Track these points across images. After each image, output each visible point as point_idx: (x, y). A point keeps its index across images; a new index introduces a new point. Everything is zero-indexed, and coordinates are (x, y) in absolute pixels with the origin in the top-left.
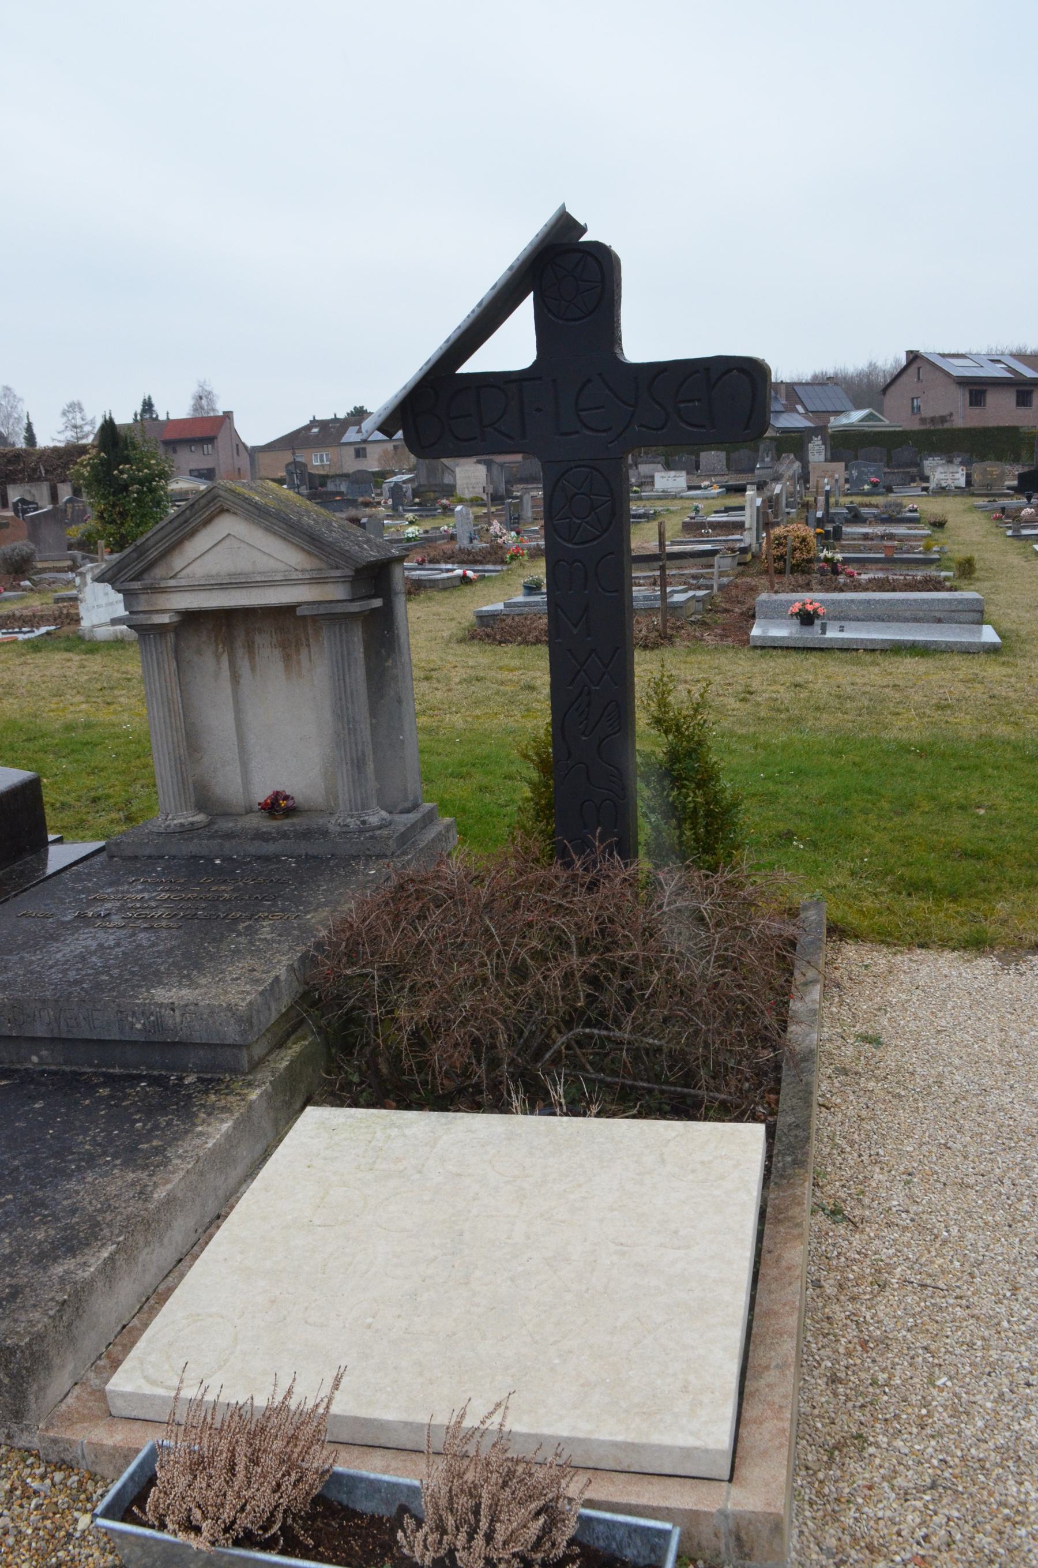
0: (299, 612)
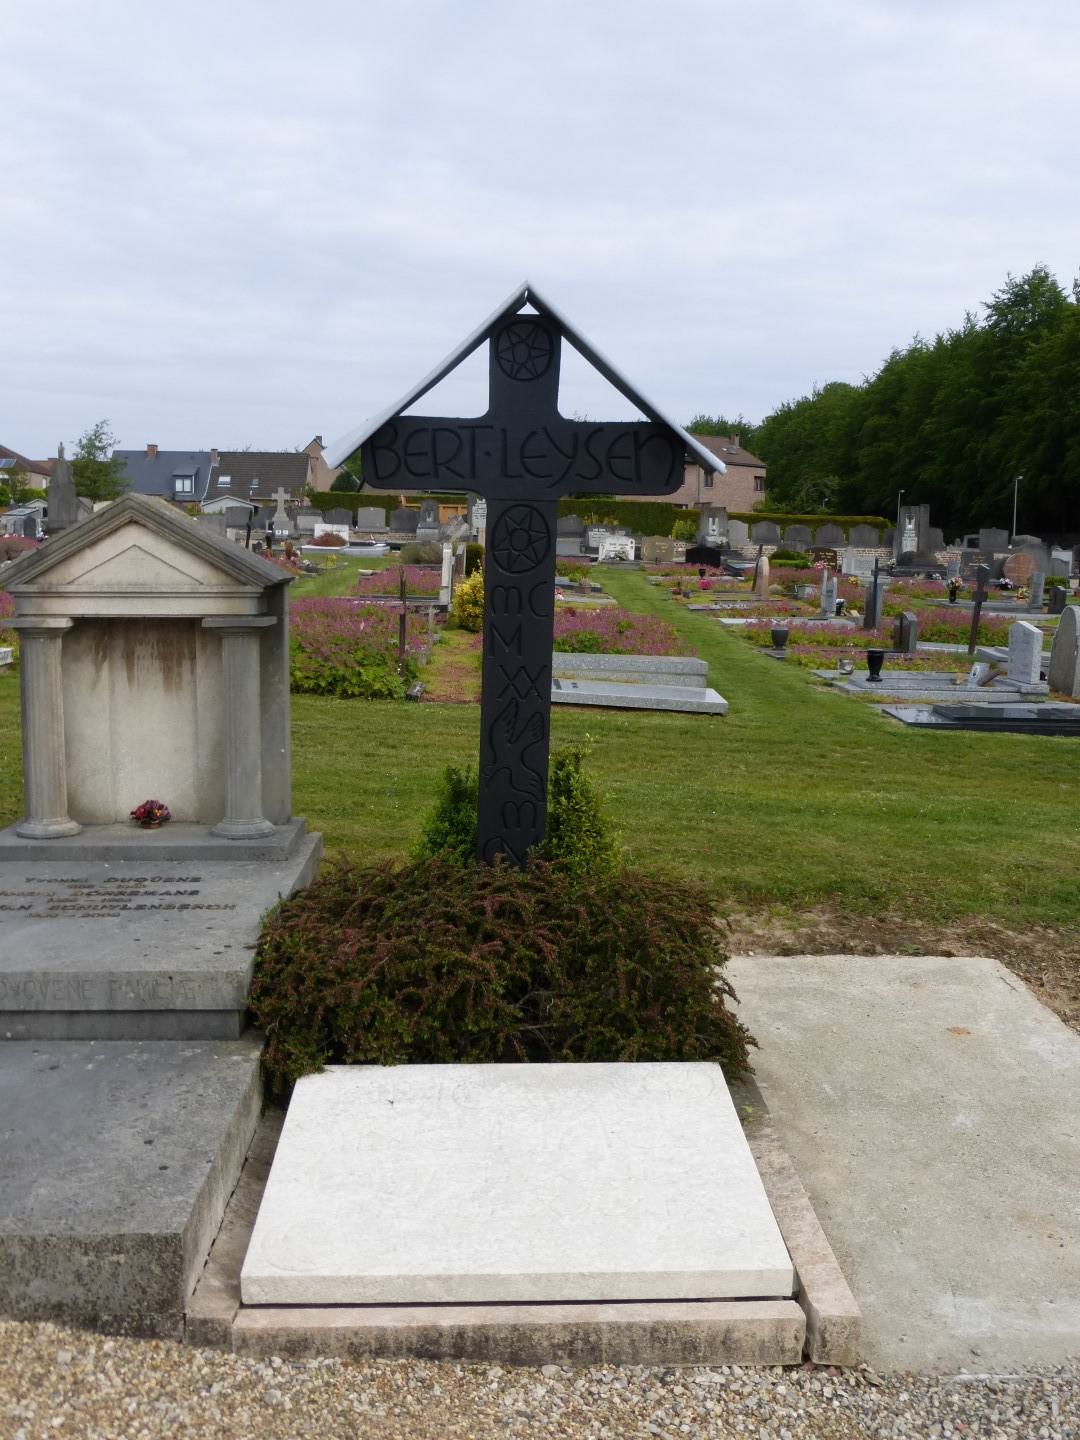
0: (205, 624)
